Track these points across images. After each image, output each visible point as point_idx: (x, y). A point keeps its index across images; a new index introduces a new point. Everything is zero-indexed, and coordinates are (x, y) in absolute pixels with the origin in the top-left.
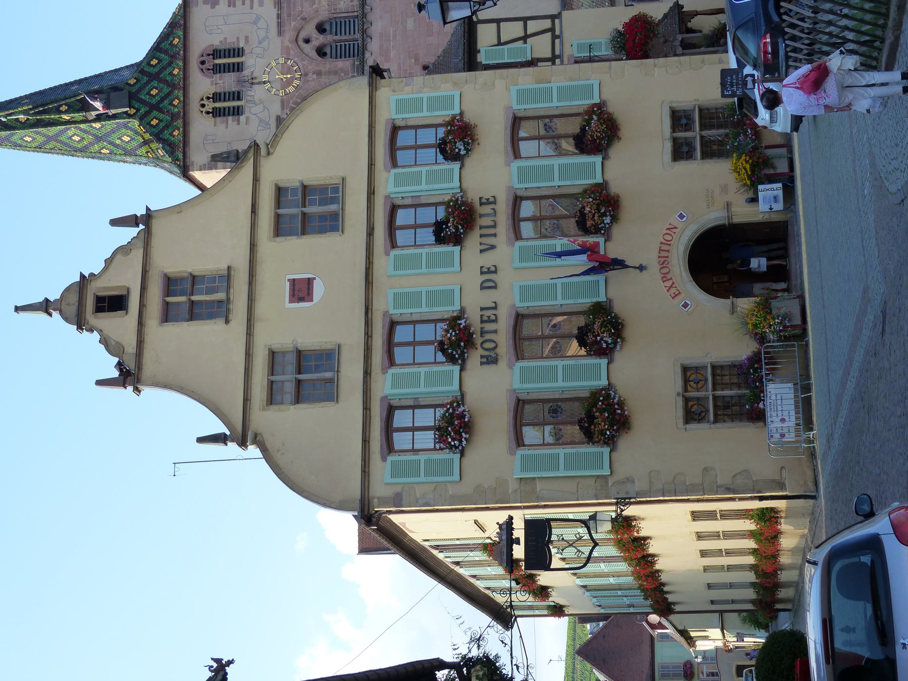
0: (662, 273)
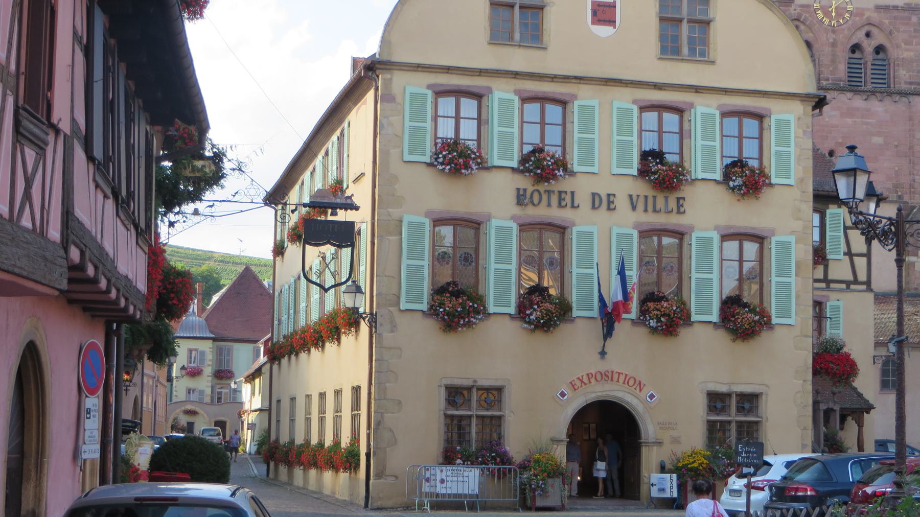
0: (596, 373)
